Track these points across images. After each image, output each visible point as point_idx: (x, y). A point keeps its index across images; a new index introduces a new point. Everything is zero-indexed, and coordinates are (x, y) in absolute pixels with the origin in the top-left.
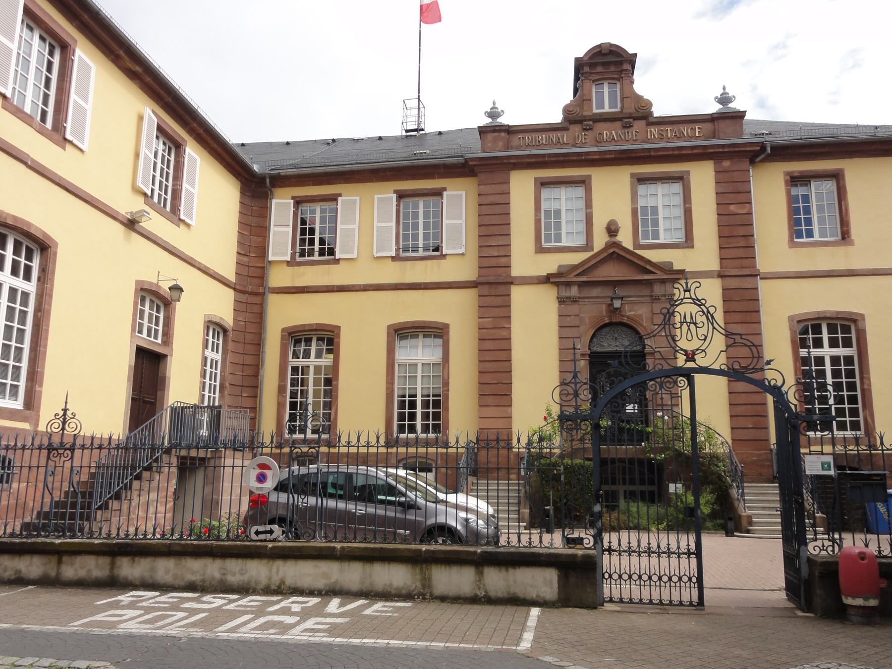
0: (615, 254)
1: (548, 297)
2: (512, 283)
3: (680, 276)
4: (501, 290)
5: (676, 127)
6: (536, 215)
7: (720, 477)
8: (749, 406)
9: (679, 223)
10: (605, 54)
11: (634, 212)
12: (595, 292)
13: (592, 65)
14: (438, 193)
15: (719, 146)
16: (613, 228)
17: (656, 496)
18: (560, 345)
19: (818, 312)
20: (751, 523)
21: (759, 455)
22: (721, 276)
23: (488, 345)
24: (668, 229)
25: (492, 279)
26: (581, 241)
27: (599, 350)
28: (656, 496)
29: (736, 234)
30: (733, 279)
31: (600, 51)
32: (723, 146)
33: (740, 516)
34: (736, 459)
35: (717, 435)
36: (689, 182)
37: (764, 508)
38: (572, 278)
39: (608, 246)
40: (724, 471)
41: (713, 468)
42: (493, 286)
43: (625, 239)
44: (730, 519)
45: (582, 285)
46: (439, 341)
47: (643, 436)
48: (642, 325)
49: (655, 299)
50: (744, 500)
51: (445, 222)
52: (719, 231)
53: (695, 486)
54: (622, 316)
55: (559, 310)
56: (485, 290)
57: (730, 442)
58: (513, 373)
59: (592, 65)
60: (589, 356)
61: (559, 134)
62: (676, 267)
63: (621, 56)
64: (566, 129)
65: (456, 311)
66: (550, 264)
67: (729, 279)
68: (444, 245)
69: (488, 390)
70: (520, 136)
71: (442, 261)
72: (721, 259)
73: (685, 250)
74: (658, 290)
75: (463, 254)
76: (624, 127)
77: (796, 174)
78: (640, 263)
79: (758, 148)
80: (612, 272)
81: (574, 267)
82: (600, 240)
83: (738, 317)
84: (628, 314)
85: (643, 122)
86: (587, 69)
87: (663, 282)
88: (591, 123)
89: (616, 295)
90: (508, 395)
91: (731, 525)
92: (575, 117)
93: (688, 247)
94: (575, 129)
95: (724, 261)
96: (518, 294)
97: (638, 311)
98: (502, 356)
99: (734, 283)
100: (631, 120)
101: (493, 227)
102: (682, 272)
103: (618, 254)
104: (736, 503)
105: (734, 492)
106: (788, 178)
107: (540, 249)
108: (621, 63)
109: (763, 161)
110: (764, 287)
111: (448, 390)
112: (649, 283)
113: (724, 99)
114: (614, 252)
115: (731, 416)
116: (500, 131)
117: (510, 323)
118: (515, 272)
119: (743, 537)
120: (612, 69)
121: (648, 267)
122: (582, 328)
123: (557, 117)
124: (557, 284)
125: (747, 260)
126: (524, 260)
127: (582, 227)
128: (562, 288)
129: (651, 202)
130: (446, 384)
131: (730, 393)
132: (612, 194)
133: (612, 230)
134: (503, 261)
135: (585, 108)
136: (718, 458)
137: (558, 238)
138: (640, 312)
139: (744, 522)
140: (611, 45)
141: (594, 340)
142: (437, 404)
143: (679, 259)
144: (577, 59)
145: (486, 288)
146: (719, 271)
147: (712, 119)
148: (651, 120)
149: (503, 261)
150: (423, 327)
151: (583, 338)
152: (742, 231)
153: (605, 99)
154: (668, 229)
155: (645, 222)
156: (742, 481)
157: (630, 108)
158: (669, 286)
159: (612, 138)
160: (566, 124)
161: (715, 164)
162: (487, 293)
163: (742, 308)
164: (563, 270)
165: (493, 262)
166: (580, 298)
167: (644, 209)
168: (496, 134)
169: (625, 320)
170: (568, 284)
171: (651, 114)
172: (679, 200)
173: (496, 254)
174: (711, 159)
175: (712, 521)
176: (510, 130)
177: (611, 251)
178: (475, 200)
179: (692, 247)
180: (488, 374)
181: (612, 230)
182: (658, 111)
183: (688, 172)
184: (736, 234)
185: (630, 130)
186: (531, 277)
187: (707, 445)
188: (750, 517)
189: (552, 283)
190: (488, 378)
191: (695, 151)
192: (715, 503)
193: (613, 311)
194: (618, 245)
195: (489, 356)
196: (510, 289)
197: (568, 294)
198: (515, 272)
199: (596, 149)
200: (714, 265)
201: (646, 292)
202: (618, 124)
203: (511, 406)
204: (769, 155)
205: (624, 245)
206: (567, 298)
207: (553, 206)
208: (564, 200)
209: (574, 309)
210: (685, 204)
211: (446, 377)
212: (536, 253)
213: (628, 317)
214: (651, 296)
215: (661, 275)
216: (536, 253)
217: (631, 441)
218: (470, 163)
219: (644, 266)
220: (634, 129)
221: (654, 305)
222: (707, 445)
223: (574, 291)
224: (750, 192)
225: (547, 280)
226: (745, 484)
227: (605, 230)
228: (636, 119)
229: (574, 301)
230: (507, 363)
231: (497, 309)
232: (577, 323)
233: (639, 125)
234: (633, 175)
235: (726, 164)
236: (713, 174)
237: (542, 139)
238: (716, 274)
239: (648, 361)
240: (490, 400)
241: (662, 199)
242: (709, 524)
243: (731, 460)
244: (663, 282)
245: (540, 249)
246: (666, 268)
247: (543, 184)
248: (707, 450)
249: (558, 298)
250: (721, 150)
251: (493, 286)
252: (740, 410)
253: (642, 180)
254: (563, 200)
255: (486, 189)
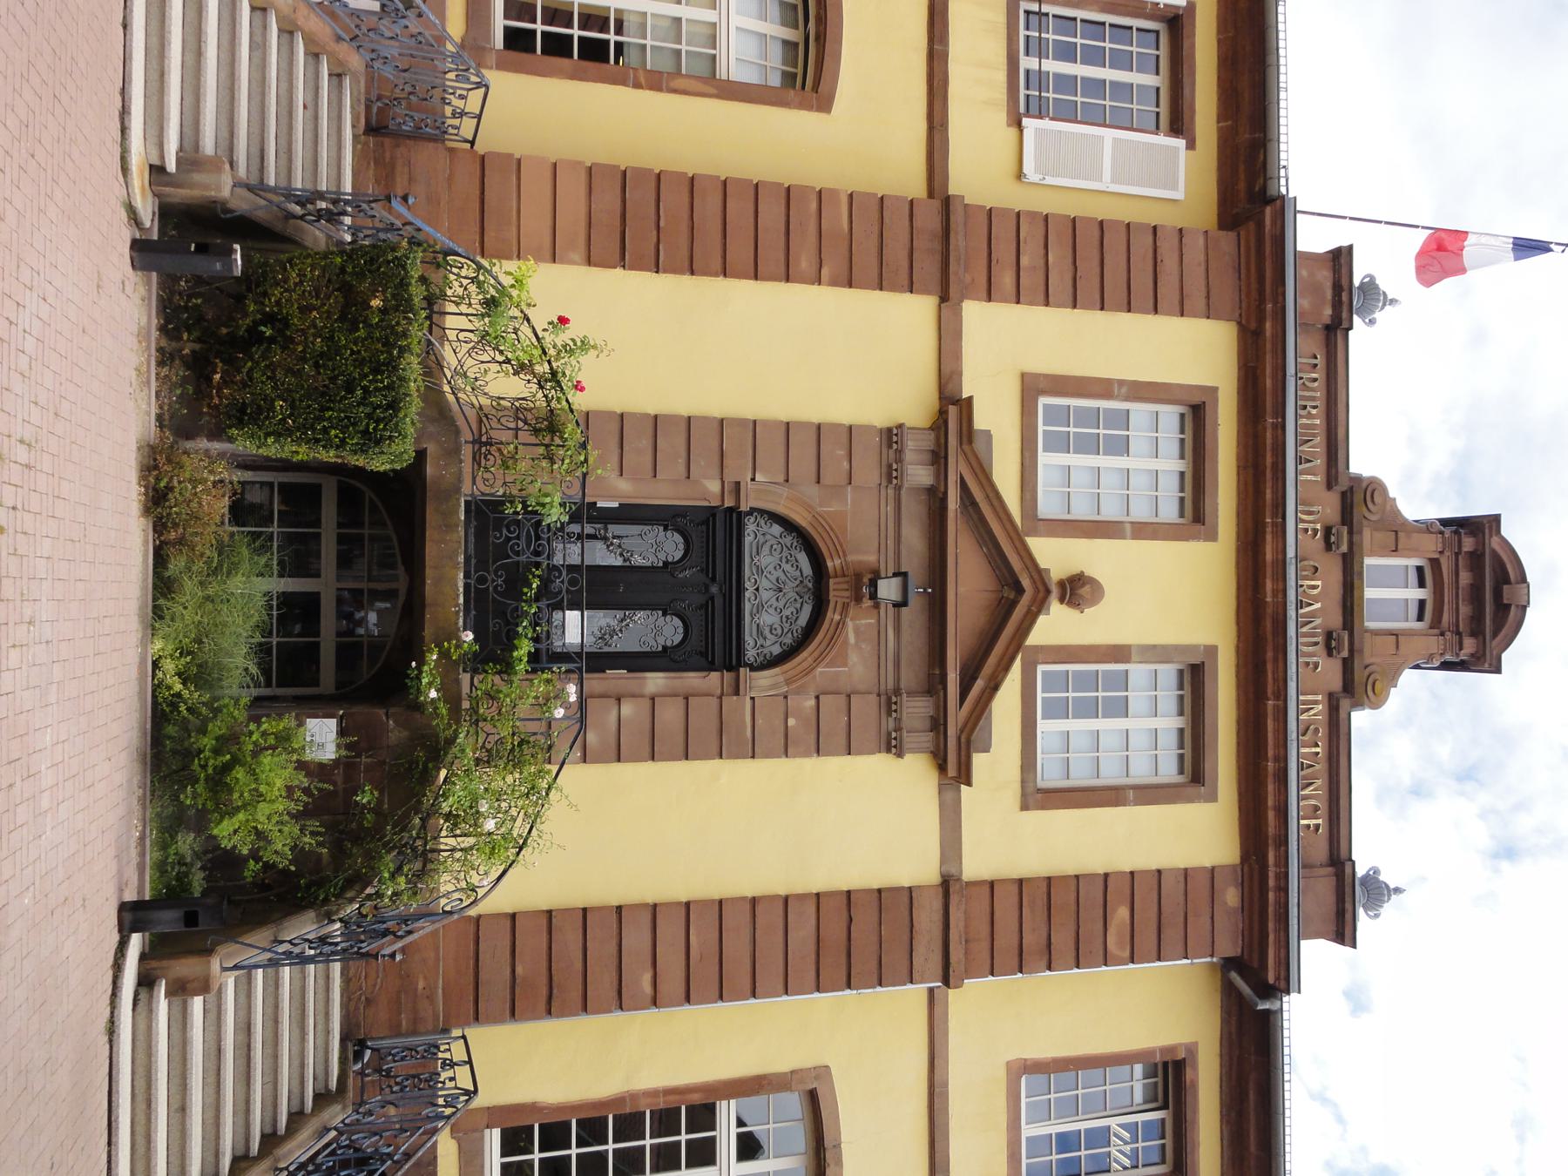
0: (1018, 592)
1: (903, 399)
2: (944, 298)
3: (952, 772)
4: (927, 266)
5: (1321, 767)
6: (1121, 383)
7: (359, 880)
8: (579, 965)
9: (1089, 775)
10: (1498, 594)
11: (1119, 653)
12: (914, 538)
13: (1476, 559)
14: (1178, 124)
15: (1284, 876)
16: (1085, 591)
17: (294, 668)
18: (766, 423)
19: (838, 1146)
20: (180, 990)
21: (431, 998)
22: (947, 884)
23: (772, 214)
24: (1075, 743)
25: (957, 241)
26: (1048, 506)
27: (748, 540)
28: (294, 668)
29: (1055, 923)
30: (937, 917)
31: (1508, 582)
32: (1283, 889)
33: (209, 952)
34: (425, 928)
35: (494, 875)
36: (1190, 800)
37: (245, 1028)
38: (956, 466)
39: (1039, 575)
40: (379, 895)
41: (389, 860)
42: (936, 245)
43: (1055, 625)
44: (191, 919)
45: (935, 499)
46: (775, 80)
47: (493, 655)
48: (818, 661)
49: (889, 702)
50: (274, 964)
51: (1109, 135)
52: (1064, 878)
53: (326, 798)
54: (845, 607)
55: (867, 429)
56: (929, 219)
57: (473, 912)
58: (687, 280)
59: (1476, 559)
60: (730, 510)
61: (1319, 462)
62: (978, 759)
63: (1495, 634)
64: (1330, 483)
65: (861, 136)
66: (995, 415)
67: (937, 904)
68: (1046, 124)
69: (640, 198)
70: (1320, 361)
71: (1002, 116)
72: (992, 884)
73: (1017, 787)
74: (916, 709)
75: (1020, 175)
76: (1329, 636)
77: (1189, 1072)
78: (992, 660)
79: (1271, 980)
80: (969, 583)
81: (983, 473)
82: (1055, 555)
83: (834, 930)
84: (850, 624)
85: (1336, 684)
86: (1468, 544)
87: (938, 724)
88: (1344, 548)
89: (907, 595)
90: (622, 258)
91: (169, 920)
92: (1357, 503)
93: (1024, 795)
94: (1328, 507)
95: (987, 889)
96: (912, 314)
97: (861, 648)
98: (740, 250)
99: (928, 917)
100: (1345, 654)
101: (1094, 262)
102: (965, 776)
103: (1013, 604)
104: (261, 937)
105: (304, 927)
106: (1181, 1055)
107: (1032, 387)
108: (1477, 631)
109: (1228, 990)
110: (909, 999)
111: (637, 86)
112: (934, 685)
113: (1377, 891)
114: (1020, 590)
115: (550, 912)
116: (1337, 304)
117: (834, 283)
118: (974, 312)
119: (118, 967)
120: (1465, 610)
121: (979, 684)
122: (812, 491)
123: (1361, 463)
124: (939, 425)
125: (986, 955)
126: (1008, 341)
127: (1082, 510)
128: (928, 441)
129: (1137, 698)
130: (656, 82)
131: (619, 908)
132: (1164, 594)
133: (1077, 590)
134: (1006, 280)
135: (1379, 535)
136: (421, 875)
137: (1061, 444)
138: (854, 658)
139: (185, 967)
140: (1523, 609)
141: (777, 529)
142: (595, 52)
143: (996, 766)
144: (1495, 520)
145: (935, 223)
146: (959, 880)
147: (1338, 860)
148: (1345, 703)
149: (1006, 280)
150: (821, 38)
151: (784, 491)
152: (1062, 939)
153: (1391, 590)
154: (1075, 743)
155: (1092, 681)
156: (346, 956)
157: (1373, 654)
158: (927, 739)
159: (1310, 597)
160: (1343, 485)
161: (1234, 866)
162: (917, 223)
163: (850, 939)
164: (979, 445)
165: (1004, 251)
166: (898, 488)
167: (1123, 681)
168: (1329, 294)
169: (832, 616)
170: (938, 458)
171: (1358, 705)
172: (1141, 772)
173: (1024, 261)
174: (1245, 857)
175: (196, 855)
176: (1335, 332)
177: (1026, 582)
178: (1168, 219)
179: (1025, 807)
180: (686, 199)
181: (1077, 590)
182: (1360, 720)
183: (1212, 797)
184: (1055, 923)
185: (1320, 649)
186: (957, 356)
187: (469, 842)
188: (204, 986)
189: (942, 413)
190: (674, 200)
191: (1271, 814)
192: (268, 867)
193: (864, 584)
194: (1039, 606)
195: (739, 210)
196: (926, 291)
197: (909, 456)
198: (974, 312)
199: (1291, 553)
200: (974, 867)
201: (911, 676)
202: (1336, 620)
203: (589, 262)
204: (1251, 1007)
205: (1042, 619)
206: (900, 452)
207: (1139, 434)
208: (1149, 465)
209: (868, 471)
210: (1136, 788)
211: (679, 83)
212: (1023, 375)
213: (840, 625)
214: (897, 692)
215: (956, 717)
216: (1023, 375)
217: (477, 600)
218: (1268, 210)
219: (981, 673)
220: (1321, 660)
221: (873, 698)
222: (469, 842)
223: (919, 474)
224: (1159, 959)
225: (952, 406)
226: (336, 968)
227: (1075, 570)
228: (1347, 665)
229: (891, 474)
230: (717, 263)
231: (874, 250)
232: (825, 480)
233: (1330, 672)
234: (1212, 651)
235: (1231, 897)
236: (1208, 864)
237: (1310, 416)
238: (953, 871)
239: (715, 675)
240: (608, 200)
241: (1145, 732)
242: (186, 843)
243: (419, 916)
244: (938, 724)
245: (1032, 387)
246: (974, 735)
247: (1197, 414)
248: (447, 842)
249: (900, 426)
250: (1271, 883)
251: (936, 245)
252: (569, 939)
253: (1195, 677)
254: (1154, 464)
255: (1195, 250)
